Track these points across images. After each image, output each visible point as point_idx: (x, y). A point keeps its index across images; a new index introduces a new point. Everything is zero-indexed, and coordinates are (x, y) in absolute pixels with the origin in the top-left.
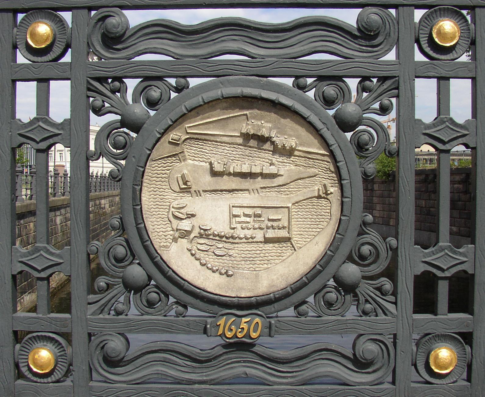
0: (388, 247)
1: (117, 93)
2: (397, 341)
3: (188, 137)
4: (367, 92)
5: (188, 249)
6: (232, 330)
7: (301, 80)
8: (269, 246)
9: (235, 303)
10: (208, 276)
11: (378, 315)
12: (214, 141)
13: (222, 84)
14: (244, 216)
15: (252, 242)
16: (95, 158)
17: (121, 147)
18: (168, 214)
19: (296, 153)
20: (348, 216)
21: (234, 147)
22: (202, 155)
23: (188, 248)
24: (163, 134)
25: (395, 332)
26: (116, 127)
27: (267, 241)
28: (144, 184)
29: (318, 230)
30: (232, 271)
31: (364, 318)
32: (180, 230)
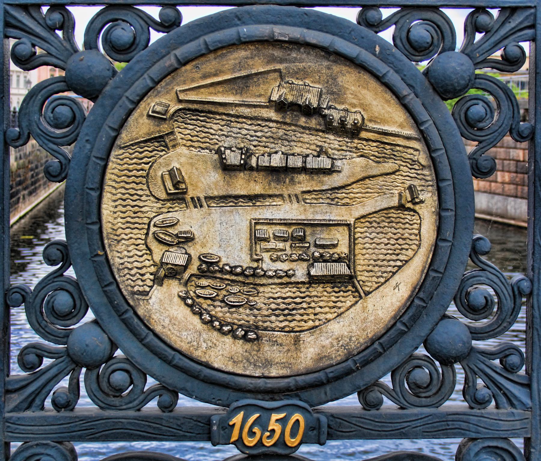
0: (516, 293)
1: (57, 32)
2: (532, 450)
3: (181, 107)
4: (480, 32)
5: (179, 296)
6: (255, 433)
7: (371, 14)
8: (317, 290)
9: (260, 387)
10: (215, 342)
11: (501, 406)
12: (225, 114)
13: (239, 19)
14: (274, 239)
15: (288, 284)
16: (21, 142)
17: (66, 124)
18: (146, 239)
19: (364, 134)
20: (450, 241)
21: (259, 125)
22: (205, 137)
23: (181, 294)
24: (137, 104)
25: (529, 436)
26: (56, 90)
27: (313, 280)
28: (106, 188)
29: (399, 263)
30: (255, 333)
31: (476, 411)
32: (167, 264)
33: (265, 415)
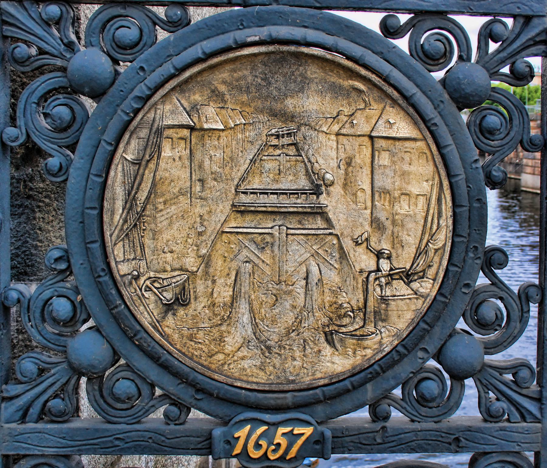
6: (261, 445)
33: (273, 428)
